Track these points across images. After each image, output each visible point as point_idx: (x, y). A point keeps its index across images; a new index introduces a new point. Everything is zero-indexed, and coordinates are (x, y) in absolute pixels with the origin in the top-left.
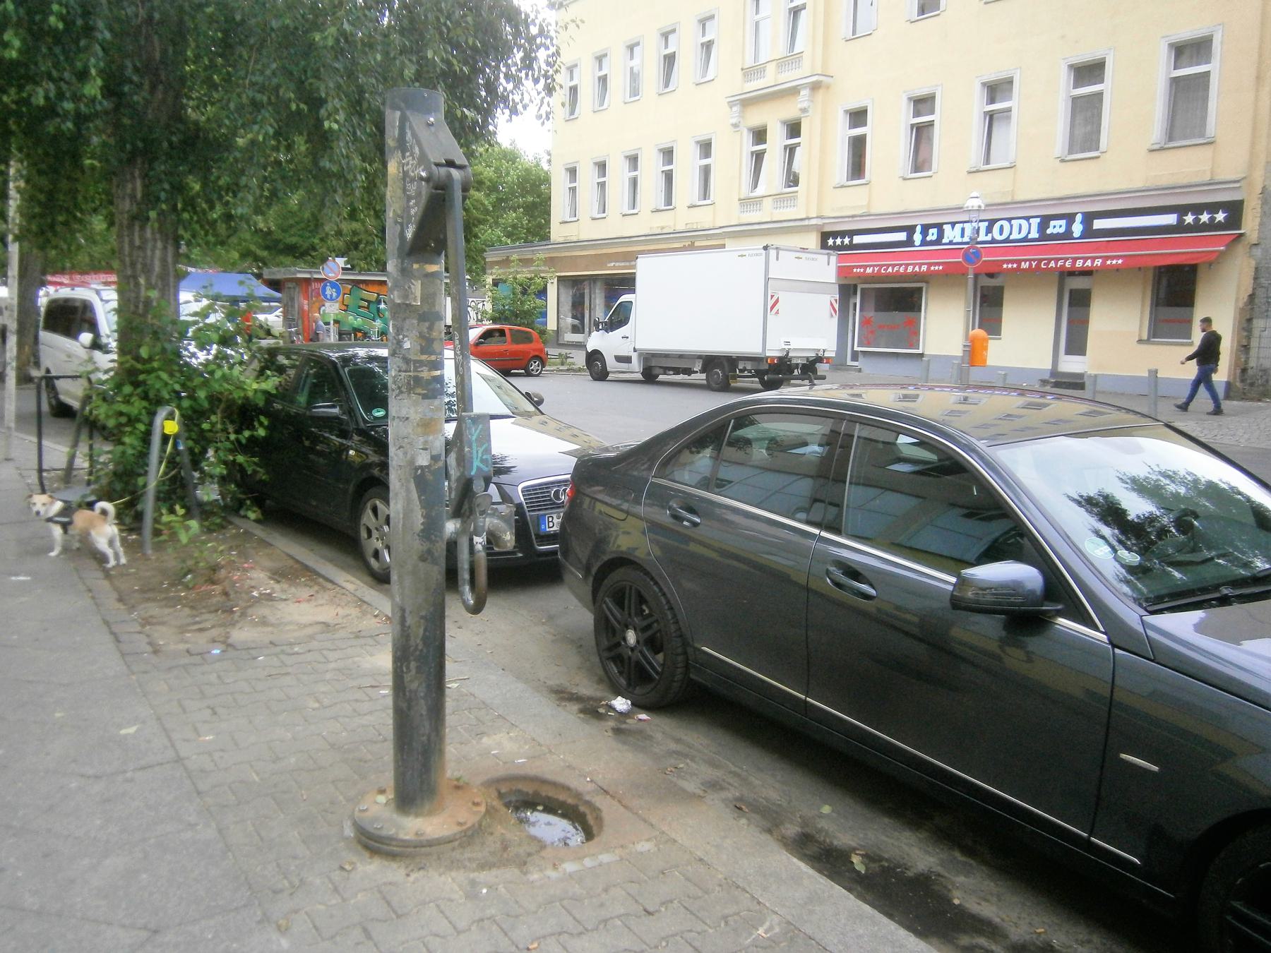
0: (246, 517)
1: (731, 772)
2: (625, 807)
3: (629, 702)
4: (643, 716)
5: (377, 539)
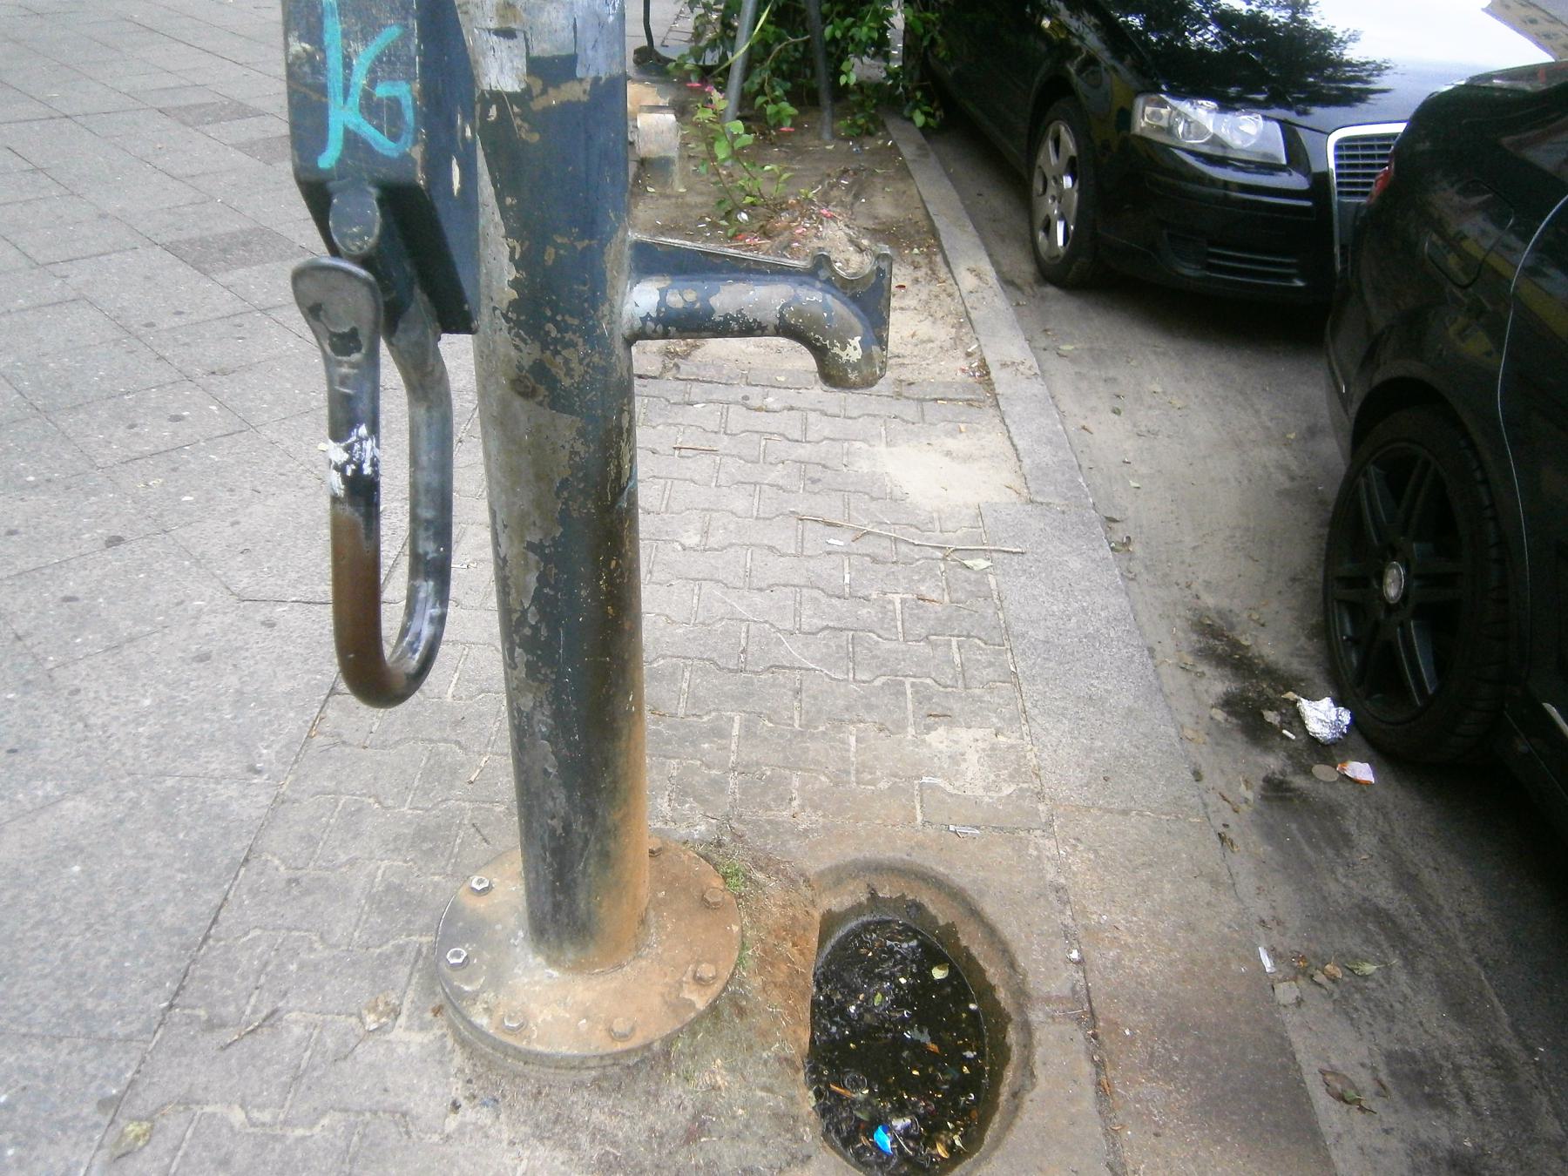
0: (911, 120)
1: (1492, 1051)
2: (1103, 1091)
3: (1346, 717)
4: (1361, 771)
5: (1054, 198)
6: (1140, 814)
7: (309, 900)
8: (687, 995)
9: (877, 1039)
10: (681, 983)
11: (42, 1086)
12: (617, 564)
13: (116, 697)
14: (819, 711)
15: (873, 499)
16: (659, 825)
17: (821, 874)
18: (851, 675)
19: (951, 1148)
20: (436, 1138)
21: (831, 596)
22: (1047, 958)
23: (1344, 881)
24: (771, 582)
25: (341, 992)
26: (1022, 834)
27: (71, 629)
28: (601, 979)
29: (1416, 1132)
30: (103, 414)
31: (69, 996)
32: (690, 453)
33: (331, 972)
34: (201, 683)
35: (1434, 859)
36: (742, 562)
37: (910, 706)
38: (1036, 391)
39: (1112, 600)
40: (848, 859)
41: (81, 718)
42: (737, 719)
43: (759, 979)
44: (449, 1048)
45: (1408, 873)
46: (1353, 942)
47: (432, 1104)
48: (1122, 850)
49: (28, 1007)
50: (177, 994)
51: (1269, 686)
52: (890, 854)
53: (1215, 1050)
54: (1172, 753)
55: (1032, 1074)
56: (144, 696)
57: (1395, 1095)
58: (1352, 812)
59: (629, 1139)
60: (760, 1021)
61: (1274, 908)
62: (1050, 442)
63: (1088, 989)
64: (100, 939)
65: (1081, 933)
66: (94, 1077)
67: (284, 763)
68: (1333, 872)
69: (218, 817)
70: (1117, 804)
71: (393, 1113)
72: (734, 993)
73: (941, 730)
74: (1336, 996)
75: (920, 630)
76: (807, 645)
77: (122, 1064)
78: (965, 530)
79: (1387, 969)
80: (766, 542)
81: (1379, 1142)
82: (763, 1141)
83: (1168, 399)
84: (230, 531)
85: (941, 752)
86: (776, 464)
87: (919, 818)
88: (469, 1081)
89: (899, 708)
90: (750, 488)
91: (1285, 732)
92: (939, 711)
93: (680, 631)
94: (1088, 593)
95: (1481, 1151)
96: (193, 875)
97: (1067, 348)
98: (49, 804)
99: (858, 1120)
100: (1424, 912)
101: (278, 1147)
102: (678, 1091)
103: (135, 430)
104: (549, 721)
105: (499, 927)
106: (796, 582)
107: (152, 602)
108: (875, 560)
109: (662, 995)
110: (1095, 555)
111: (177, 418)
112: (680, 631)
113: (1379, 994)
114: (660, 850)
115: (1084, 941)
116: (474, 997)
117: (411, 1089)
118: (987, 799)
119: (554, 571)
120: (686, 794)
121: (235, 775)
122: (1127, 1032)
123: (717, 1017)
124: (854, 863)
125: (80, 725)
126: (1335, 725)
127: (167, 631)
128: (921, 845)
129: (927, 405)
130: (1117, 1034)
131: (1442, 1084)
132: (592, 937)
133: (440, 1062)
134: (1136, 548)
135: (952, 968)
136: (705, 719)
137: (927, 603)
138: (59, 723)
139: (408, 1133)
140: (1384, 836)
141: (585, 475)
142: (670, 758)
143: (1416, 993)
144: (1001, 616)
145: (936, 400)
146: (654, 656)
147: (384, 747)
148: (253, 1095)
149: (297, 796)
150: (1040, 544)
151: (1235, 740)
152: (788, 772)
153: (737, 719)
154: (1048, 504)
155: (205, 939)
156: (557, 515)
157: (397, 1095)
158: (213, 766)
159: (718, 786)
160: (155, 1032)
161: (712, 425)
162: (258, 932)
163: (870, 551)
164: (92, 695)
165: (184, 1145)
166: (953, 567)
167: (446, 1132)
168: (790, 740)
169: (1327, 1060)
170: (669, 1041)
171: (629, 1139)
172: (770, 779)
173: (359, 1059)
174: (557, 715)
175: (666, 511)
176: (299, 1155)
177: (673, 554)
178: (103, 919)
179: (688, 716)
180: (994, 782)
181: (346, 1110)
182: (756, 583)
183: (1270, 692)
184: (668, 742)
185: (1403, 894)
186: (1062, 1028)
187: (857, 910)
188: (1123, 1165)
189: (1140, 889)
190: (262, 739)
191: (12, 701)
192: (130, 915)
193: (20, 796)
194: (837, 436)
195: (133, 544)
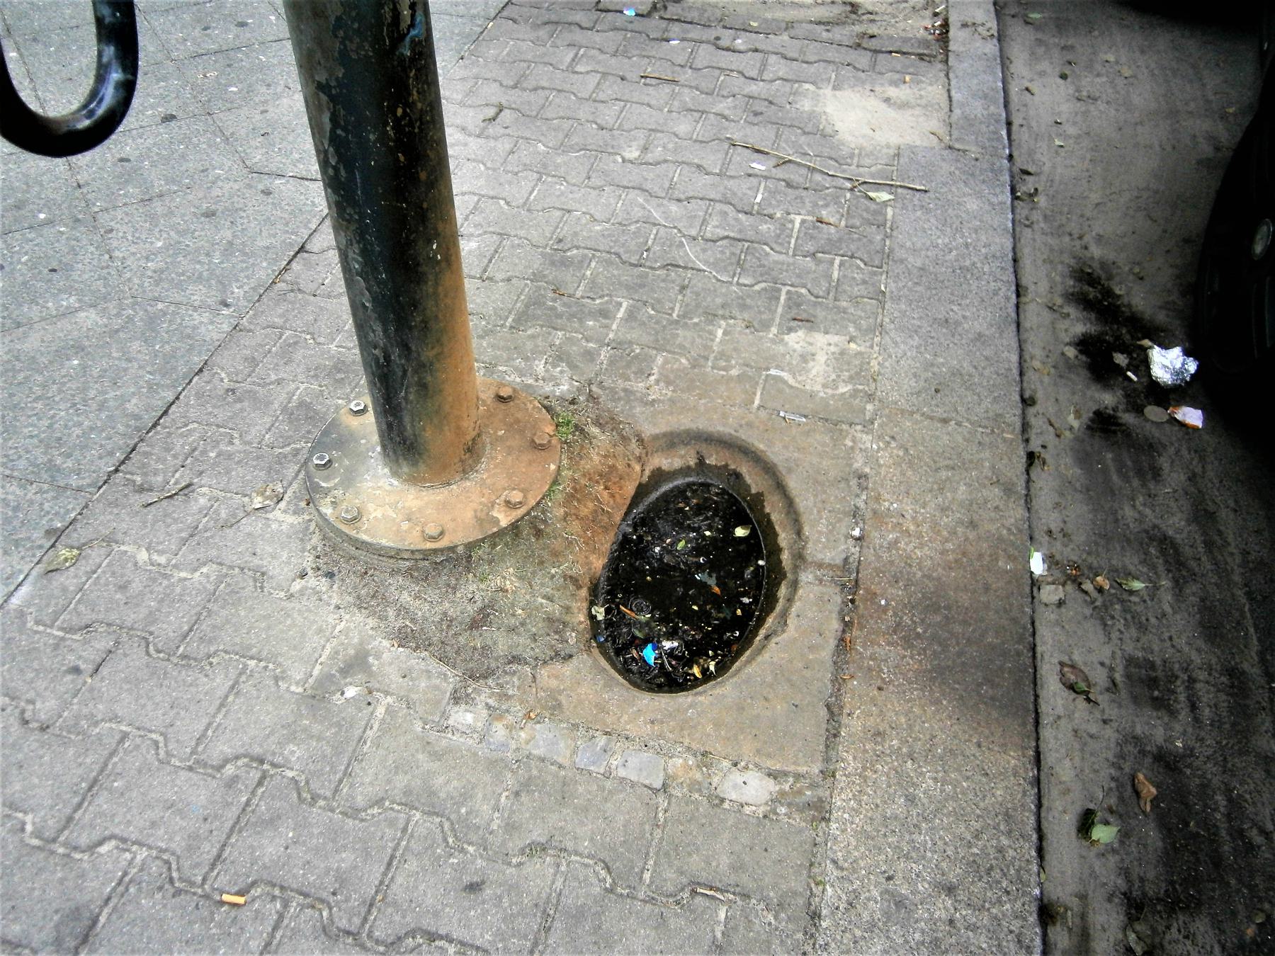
1: (1233, 673)
2: (843, 645)
3: (1192, 366)
6: (959, 424)
7: (238, 406)
8: (495, 514)
9: (670, 576)
10: (493, 504)
11: (10, 513)
12: (404, 111)
13: (138, 238)
14: (698, 306)
15: (805, 133)
16: (530, 381)
17: (656, 438)
18: (736, 279)
19: (705, 671)
20: (282, 594)
21: (739, 211)
22: (831, 532)
23: (1141, 508)
24: (691, 194)
25: (244, 477)
26: (844, 427)
27: (119, 184)
28: (431, 491)
29: (1133, 727)
30: (187, 17)
31: (45, 453)
32: (654, 82)
33: (239, 462)
34: (203, 233)
35: (1236, 502)
36: (671, 176)
37: (780, 310)
38: (987, 51)
39: (997, 240)
40: (682, 428)
41: (108, 252)
42: (625, 305)
43: (562, 510)
44: (312, 529)
45: (1205, 510)
46: (1131, 561)
47: (286, 569)
48: (931, 452)
49: (15, 457)
50: (123, 462)
51: (1129, 332)
52: (720, 428)
53: (958, 629)
54: (1006, 377)
55: (785, 624)
56: (159, 240)
57: (1124, 694)
58: (1172, 450)
59: (425, 619)
60: (557, 544)
61: (1065, 522)
62: (985, 97)
63: (859, 561)
64: (78, 415)
65: (868, 515)
66: (48, 513)
67: (249, 301)
68: (1133, 500)
69: (189, 337)
70: (940, 412)
71: (256, 571)
72: (535, 517)
73: (801, 333)
74: (1098, 603)
75: (810, 247)
76: (704, 250)
77: (70, 507)
78: (880, 167)
79: (1154, 589)
80: (696, 161)
81: (1094, 729)
82: (534, 638)
83: (1117, 68)
84: (258, 117)
85: (794, 351)
86: (728, 97)
87: (757, 402)
88: (318, 557)
89: (770, 310)
90: (697, 115)
91: (1129, 374)
92: (804, 316)
93: (598, 228)
94: (976, 231)
95: (1190, 752)
96: (158, 377)
97: (1035, 16)
98: (69, 312)
99: (634, 637)
100: (1209, 545)
101: (165, 583)
102: (472, 587)
103: (208, 31)
104: (360, 259)
105: (363, 441)
106: (712, 196)
107: (184, 168)
108: (789, 185)
109: (475, 511)
110: (995, 200)
111: (242, 25)
112: (598, 228)
113: (1139, 608)
114: (510, 397)
115: (869, 523)
116: (327, 492)
117: (274, 557)
118: (822, 394)
119: (342, 112)
120: (561, 359)
121: (209, 306)
122: (883, 602)
123: (517, 535)
124: (688, 432)
125: (107, 257)
126: (1178, 373)
127: (188, 191)
128: (750, 425)
129: (881, 56)
130: (873, 603)
131: (1174, 692)
132: (419, 454)
133: (302, 540)
134: (1041, 200)
135: (753, 531)
136: (598, 301)
137: (824, 226)
138: (92, 253)
139: (262, 588)
140: (1194, 475)
141: (358, 14)
142: (557, 329)
143: (1175, 613)
144: (888, 243)
145: (891, 52)
146: (569, 246)
147: (329, 297)
148: (158, 543)
149: (252, 327)
150: (944, 184)
151: (1078, 374)
152: (655, 352)
153: (625, 305)
154: (964, 151)
155: (154, 426)
156: (336, 54)
157: (261, 559)
158: (195, 297)
159: (590, 356)
160: (100, 488)
161: (680, 60)
162: (196, 425)
163: (786, 177)
164: (121, 234)
165: (99, 570)
166: (858, 197)
167: (291, 591)
168: (664, 327)
169: (1070, 655)
170: (470, 546)
171: (425, 619)
172: (637, 357)
173: (241, 528)
174: (365, 252)
175: (618, 129)
176: (178, 590)
177: (612, 165)
178: (85, 401)
179: (583, 297)
180: (834, 380)
181: (220, 564)
182: (677, 194)
183: (1127, 337)
184: (559, 316)
185: (1194, 527)
186: (824, 590)
187: (685, 471)
188: (841, 708)
189: (935, 487)
190: (237, 281)
191: (62, 233)
192: (106, 401)
193: (50, 304)
194: (790, 77)
195: (183, 122)
